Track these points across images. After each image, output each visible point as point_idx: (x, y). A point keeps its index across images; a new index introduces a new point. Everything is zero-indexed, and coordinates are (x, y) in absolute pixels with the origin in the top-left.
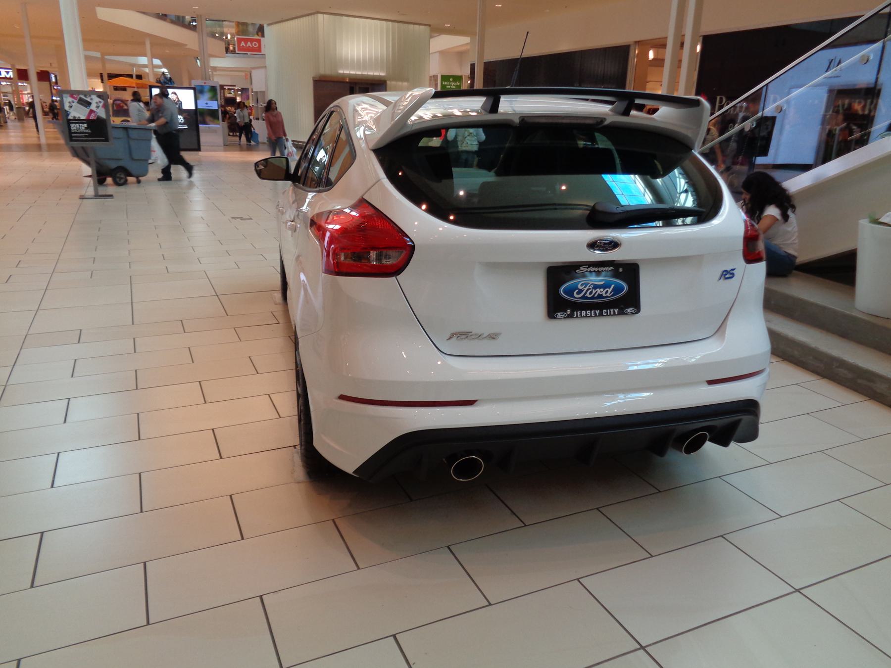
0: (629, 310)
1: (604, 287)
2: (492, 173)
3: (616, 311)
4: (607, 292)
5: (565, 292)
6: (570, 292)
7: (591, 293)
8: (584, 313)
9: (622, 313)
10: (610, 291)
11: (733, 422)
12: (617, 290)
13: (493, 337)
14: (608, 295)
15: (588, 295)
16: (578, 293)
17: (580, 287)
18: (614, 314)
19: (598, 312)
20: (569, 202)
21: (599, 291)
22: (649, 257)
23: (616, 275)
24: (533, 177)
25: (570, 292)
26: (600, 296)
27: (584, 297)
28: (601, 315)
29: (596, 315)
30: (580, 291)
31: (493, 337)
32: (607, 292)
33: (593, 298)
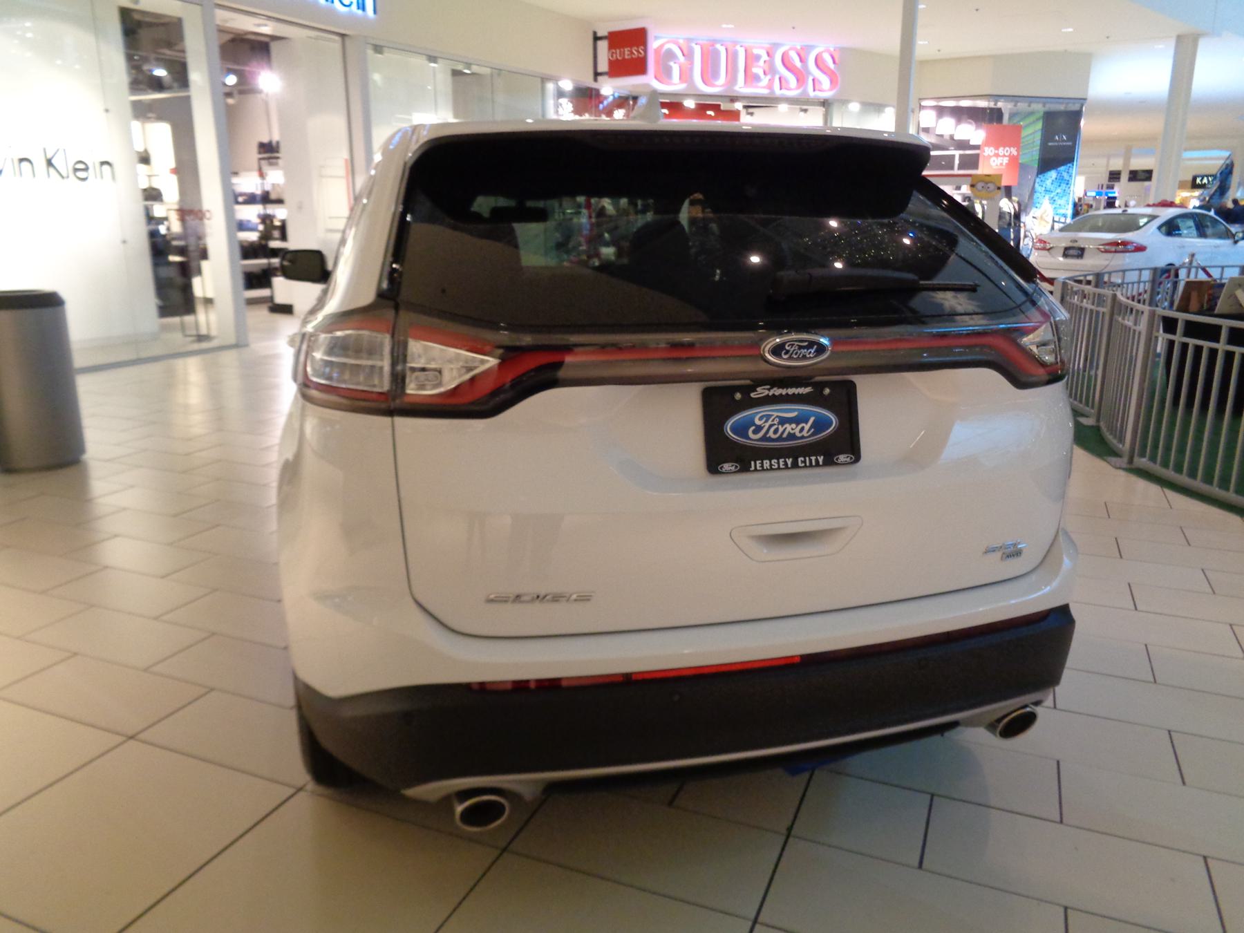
0: (842, 458)
1: (797, 421)
2: (975, 303)
3: (821, 459)
4: (802, 429)
5: (733, 429)
6: (741, 429)
7: (776, 431)
8: (766, 463)
9: (829, 462)
10: (807, 427)
11: (1013, 661)
12: (820, 425)
13: (584, 598)
14: (805, 433)
15: (771, 434)
16: (755, 432)
17: (757, 422)
18: (811, 465)
19: (789, 461)
20: (1074, 475)
21: (789, 428)
22: (878, 376)
23: (814, 399)
24: (334, 754)
25: (741, 429)
26: (792, 436)
27: (764, 438)
28: (795, 465)
29: (786, 467)
30: (759, 429)
31: (584, 598)
32: (802, 429)
33: (780, 439)
